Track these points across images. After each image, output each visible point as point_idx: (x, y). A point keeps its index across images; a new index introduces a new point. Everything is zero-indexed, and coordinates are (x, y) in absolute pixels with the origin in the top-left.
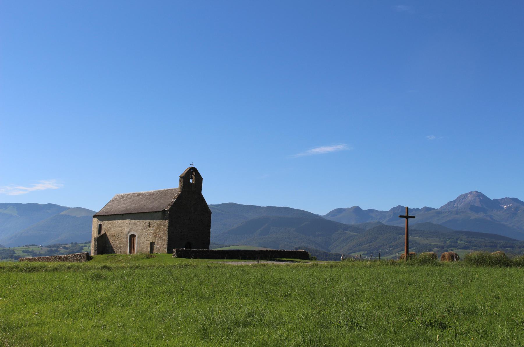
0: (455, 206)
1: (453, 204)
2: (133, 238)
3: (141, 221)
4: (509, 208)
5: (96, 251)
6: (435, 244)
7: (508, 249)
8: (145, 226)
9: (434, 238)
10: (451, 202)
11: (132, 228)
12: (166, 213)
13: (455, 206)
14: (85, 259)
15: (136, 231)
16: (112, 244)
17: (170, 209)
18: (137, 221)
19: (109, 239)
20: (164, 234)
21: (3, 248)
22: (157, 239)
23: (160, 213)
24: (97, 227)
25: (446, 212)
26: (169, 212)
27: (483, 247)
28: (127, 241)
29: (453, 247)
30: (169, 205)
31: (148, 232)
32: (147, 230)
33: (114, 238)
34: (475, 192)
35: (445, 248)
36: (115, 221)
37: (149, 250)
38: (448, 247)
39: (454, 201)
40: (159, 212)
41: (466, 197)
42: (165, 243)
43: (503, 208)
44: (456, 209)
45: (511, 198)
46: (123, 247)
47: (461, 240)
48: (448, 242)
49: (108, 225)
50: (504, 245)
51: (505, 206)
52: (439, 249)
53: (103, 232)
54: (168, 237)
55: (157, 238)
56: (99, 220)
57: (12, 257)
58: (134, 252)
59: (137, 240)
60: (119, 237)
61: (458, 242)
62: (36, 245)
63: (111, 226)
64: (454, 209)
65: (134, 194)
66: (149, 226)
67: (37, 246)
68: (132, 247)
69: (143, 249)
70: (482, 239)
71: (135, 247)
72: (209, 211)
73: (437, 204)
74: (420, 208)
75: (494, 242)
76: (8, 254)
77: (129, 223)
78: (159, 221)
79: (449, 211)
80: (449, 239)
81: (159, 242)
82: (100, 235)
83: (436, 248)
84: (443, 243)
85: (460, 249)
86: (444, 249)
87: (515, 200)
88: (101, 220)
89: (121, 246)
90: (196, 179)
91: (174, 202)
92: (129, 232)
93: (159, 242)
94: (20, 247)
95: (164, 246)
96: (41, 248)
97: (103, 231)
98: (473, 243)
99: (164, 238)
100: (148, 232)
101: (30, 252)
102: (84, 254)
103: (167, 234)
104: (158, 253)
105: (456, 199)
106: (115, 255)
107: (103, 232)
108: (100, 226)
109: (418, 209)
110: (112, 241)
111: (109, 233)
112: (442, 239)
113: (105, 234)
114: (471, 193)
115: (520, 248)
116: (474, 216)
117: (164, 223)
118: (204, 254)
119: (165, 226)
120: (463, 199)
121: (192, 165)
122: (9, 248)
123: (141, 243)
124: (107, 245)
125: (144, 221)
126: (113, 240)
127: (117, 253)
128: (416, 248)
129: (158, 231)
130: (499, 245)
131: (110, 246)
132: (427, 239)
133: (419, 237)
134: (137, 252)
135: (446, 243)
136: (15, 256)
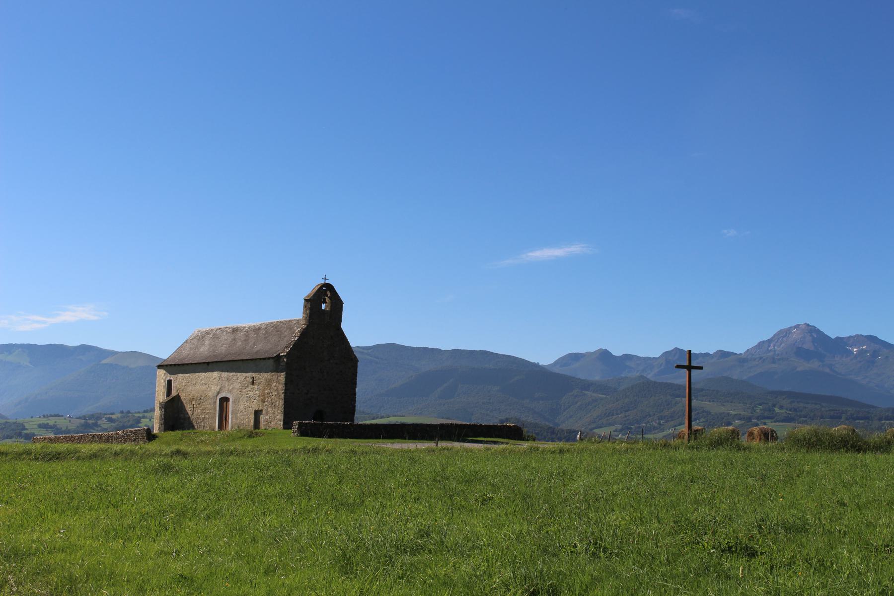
0: (771, 350)
2: (225, 403)
4: (861, 352)
5: (163, 426)
6: (736, 413)
7: (859, 423)
11: (223, 386)
12: (282, 360)
15: (230, 391)
16: (190, 414)
17: (288, 353)
19: (185, 405)
20: (278, 396)
22: (266, 405)
23: (271, 361)
25: (755, 359)
26: (285, 360)
29: (768, 418)
31: (251, 393)
32: (249, 389)
33: (193, 402)
34: (804, 326)
35: (753, 420)
37: (252, 423)
38: (758, 418)
39: (769, 341)
40: (269, 358)
41: (789, 334)
42: (279, 412)
43: (852, 352)
44: (772, 353)
46: (208, 418)
47: (781, 407)
49: (183, 381)
51: (855, 350)
52: (743, 422)
53: (174, 393)
55: (266, 403)
57: (20, 435)
58: (227, 426)
63: (188, 383)
66: (253, 383)
67: (62, 416)
68: (224, 418)
69: (243, 422)
70: (816, 404)
73: (740, 345)
74: (711, 353)
75: (836, 410)
77: (218, 378)
79: (761, 358)
80: (760, 404)
81: (270, 409)
83: (738, 420)
84: (750, 411)
85: (779, 421)
86: (751, 421)
87: (872, 339)
88: (171, 373)
90: (332, 303)
92: (218, 393)
93: (270, 409)
96: (70, 421)
97: (175, 391)
99: (277, 402)
100: (251, 393)
101: (51, 427)
103: (282, 396)
105: (773, 338)
107: (174, 393)
108: (170, 382)
109: (707, 354)
112: (748, 405)
114: (797, 326)
115: (880, 419)
116: (803, 366)
117: (277, 377)
119: (279, 383)
120: (783, 337)
122: (15, 421)
123: (239, 412)
124: (182, 415)
125: (244, 374)
126: (191, 406)
128: (704, 420)
130: (844, 415)
131: (186, 416)
133: (710, 401)
134: (232, 427)
135: (755, 411)
136: (26, 434)
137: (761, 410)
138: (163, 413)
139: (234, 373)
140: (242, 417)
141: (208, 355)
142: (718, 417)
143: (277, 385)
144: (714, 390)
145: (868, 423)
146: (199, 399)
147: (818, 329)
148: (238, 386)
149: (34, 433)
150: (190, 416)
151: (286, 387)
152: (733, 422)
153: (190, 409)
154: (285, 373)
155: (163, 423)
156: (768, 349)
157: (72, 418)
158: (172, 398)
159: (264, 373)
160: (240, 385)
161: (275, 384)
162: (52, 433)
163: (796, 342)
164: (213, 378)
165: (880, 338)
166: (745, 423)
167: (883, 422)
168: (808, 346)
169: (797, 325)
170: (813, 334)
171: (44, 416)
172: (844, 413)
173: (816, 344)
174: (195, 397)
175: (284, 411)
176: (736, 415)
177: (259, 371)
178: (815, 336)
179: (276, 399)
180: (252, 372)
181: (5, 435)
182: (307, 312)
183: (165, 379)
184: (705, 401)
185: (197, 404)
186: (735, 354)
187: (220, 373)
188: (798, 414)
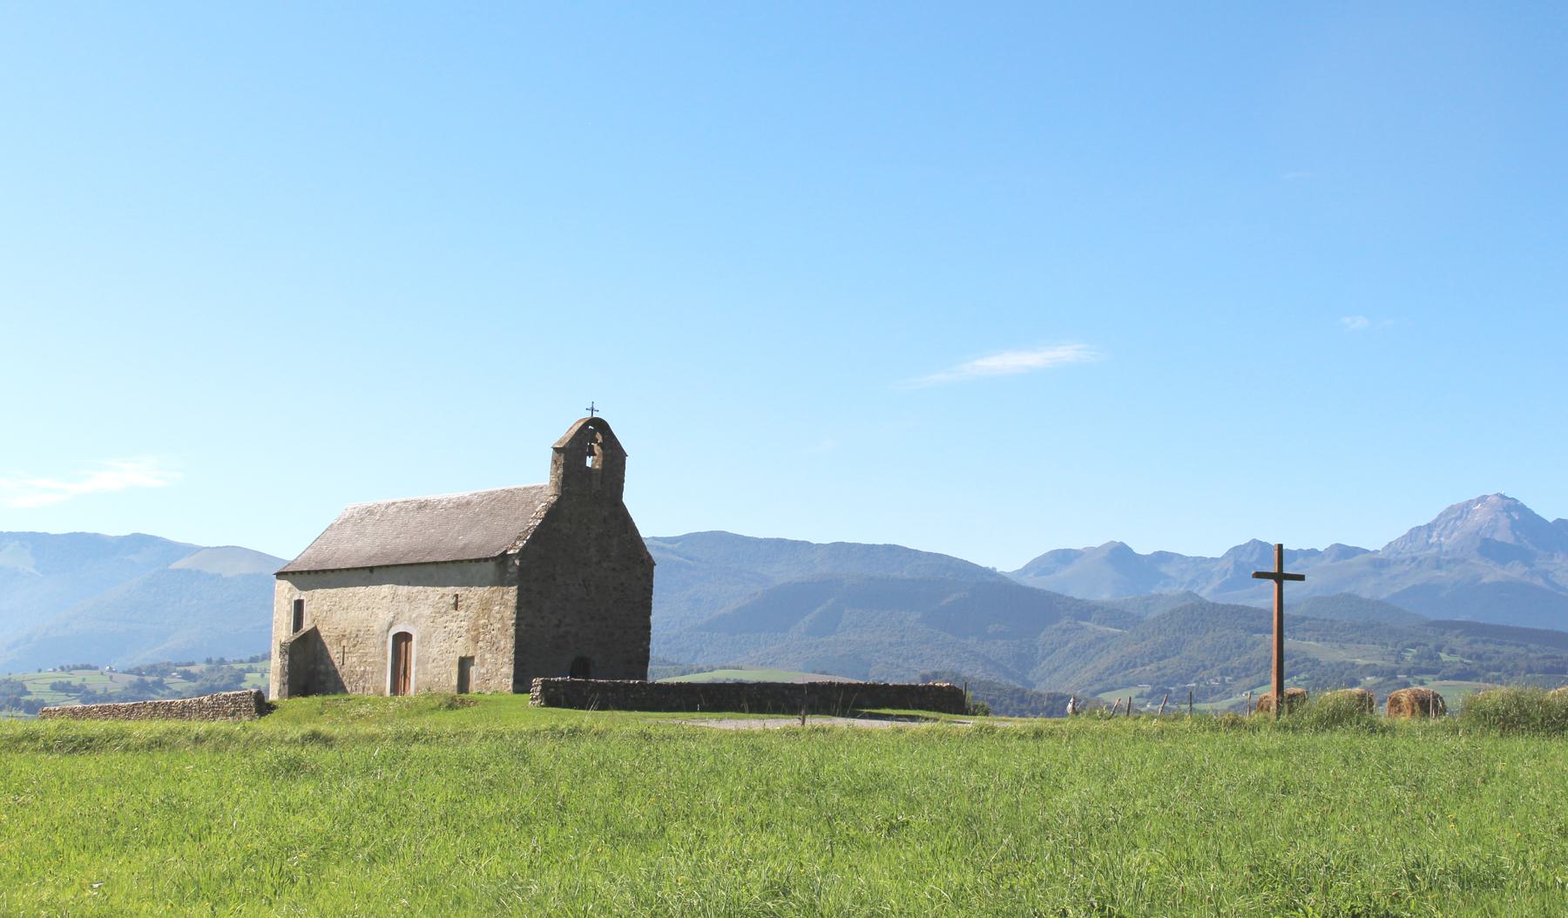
0: (1433, 543)
2: (404, 644)
3: (430, 589)
5: (287, 686)
6: (1367, 662)
12: (510, 563)
15: (413, 622)
16: (337, 664)
17: (523, 550)
19: (328, 647)
20: (504, 629)
24: (288, 608)
26: (517, 562)
27: (1523, 672)
28: (385, 654)
29: (1427, 672)
31: (453, 626)
33: (344, 643)
37: (455, 682)
38: (1408, 672)
39: (1430, 527)
40: (486, 560)
41: (1468, 513)
42: (507, 660)
44: (1434, 550)
46: (372, 673)
47: (1452, 652)
48: (1410, 656)
49: (324, 602)
52: (1381, 679)
53: (307, 626)
54: (516, 641)
55: (480, 644)
56: (294, 588)
57: (16, 704)
59: (418, 650)
61: (1443, 655)
62: (93, 665)
63: (334, 605)
64: (1428, 552)
66: (456, 606)
67: (96, 668)
68: (402, 673)
69: (437, 679)
70: (1518, 646)
71: (410, 673)
73: (1375, 536)
74: (1321, 549)
77: (390, 597)
78: (486, 589)
79: (1414, 559)
80: (1413, 646)
81: (488, 656)
84: (1393, 659)
86: (1397, 678)
88: (302, 588)
90: (605, 455)
91: (536, 530)
92: (391, 625)
93: (488, 656)
94: (42, 674)
96: (111, 677)
97: (309, 622)
99: (502, 643)
100: (453, 626)
101: (76, 690)
102: (246, 694)
103: (512, 631)
105: (1437, 520)
106: (346, 697)
107: (307, 626)
108: (299, 605)
109: (1313, 552)
111: (327, 629)
113: (315, 632)
114: (1483, 499)
116: (1493, 573)
117: (503, 595)
120: (1456, 519)
122: (7, 677)
123: (431, 660)
124: (322, 667)
126: (340, 649)
128: (1307, 676)
129: (482, 622)
131: (330, 668)
133: (1317, 640)
134: (417, 689)
135: (1403, 659)
136: (28, 702)
137: (1414, 657)
138: (287, 662)
140: (436, 671)
146: (354, 635)
149: (43, 700)
151: (518, 614)
152: (1362, 680)
154: (516, 587)
155: (286, 681)
157: (116, 671)
160: (431, 609)
162: (78, 700)
164: (382, 596)
166: (1383, 681)
168: (1503, 536)
169: (1484, 496)
171: (62, 669)
173: (1518, 533)
174: (348, 631)
177: (469, 584)
178: (1517, 518)
179: (499, 637)
183: (292, 597)
185: (350, 645)
186: (1365, 551)
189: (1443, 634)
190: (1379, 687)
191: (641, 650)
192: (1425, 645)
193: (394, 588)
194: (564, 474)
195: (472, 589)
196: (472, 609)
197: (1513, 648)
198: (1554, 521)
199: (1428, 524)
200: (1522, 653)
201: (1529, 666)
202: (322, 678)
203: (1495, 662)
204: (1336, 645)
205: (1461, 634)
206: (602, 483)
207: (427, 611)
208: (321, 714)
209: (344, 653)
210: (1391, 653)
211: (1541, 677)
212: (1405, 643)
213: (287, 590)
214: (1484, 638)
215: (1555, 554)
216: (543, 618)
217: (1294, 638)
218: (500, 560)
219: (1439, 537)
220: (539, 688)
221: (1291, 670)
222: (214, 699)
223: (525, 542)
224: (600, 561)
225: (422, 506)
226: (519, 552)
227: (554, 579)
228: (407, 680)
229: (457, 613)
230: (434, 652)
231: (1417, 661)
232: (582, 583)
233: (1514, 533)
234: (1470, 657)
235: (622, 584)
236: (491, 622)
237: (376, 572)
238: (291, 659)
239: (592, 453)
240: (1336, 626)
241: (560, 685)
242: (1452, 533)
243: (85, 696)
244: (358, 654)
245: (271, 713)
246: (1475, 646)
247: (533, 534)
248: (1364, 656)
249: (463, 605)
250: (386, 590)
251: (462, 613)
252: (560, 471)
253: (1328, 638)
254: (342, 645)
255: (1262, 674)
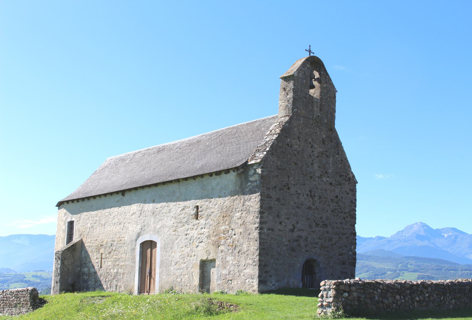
0: (403, 236)
1: (401, 233)
2: (149, 250)
3: (172, 204)
4: (449, 237)
5: (59, 284)
6: (388, 268)
7: (451, 272)
8: (183, 216)
9: (387, 263)
10: (400, 231)
11: (146, 223)
12: (252, 172)
13: (403, 235)
14: (26, 304)
15: (158, 232)
16: (96, 267)
17: (264, 160)
18: (159, 205)
19: (90, 254)
20: (247, 233)
21: (15, 273)
22: (222, 251)
23: (232, 176)
24: (64, 227)
25: (396, 240)
26: (259, 171)
27: (431, 270)
28: (134, 259)
29: (405, 270)
30: (258, 151)
31: (194, 233)
32: (189, 227)
33: (102, 251)
34: (420, 223)
35: (397, 271)
36: (105, 210)
37: (196, 281)
38: (399, 270)
39: (402, 231)
40: (227, 171)
41: (412, 227)
42: (251, 262)
43: (444, 237)
44: (404, 237)
45: (450, 227)
46: (123, 274)
47: (411, 265)
48: (400, 266)
49: (88, 221)
50: (448, 268)
51: (446, 235)
52: (392, 272)
53: (76, 239)
54: (260, 244)
55: (222, 248)
56: (68, 213)
57: (22, 281)
58: (152, 286)
59: (161, 255)
60: (114, 248)
61: (408, 266)
62: (44, 270)
63: (95, 223)
64: (402, 238)
65: (149, 151)
66: (197, 216)
67: (44, 271)
68: (147, 274)
69: (179, 280)
70: (428, 263)
71: (155, 274)
72: (351, 175)
73: (388, 233)
74: (373, 237)
75: (439, 266)
76: (19, 278)
77: (138, 213)
78: (227, 198)
79: (399, 240)
80: (400, 263)
81: (229, 258)
82: (70, 245)
83: (389, 271)
84: (395, 267)
85: (410, 272)
86: (397, 272)
87: (454, 230)
88: (73, 212)
89: (118, 270)
90: (322, 88)
91: (273, 144)
92: (138, 236)
93: (229, 258)
94: (30, 273)
95: (247, 271)
96: (48, 273)
97: (77, 237)
98: (421, 267)
99: (245, 246)
100: (194, 233)
101: (39, 277)
102: (24, 291)
103: (256, 234)
104: (226, 290)
105: (404, 229)
106: (103, 294)
107: (76, 239)
108: (71, 224)
109: (371, 238)
110: (97, 258)
111: (89, 241)
112: (394, 264)
113: (81, 243)
114: (416, 223)
115: (462, 270)
116: (420, 243)
117: (244, 202)
118: (417, 299)
119: (248, 212)
120: (410, 229)
121: (310, 51)
122: (20, 274)
123: (173, 263)
124: (86, 270)
125: (180, 203)
126: (99, 256)
127: (107, 288)
128: (372, 272)
129: (223, 228)
130: (443, 268)
131: (92, 270)
132: (382, 264)
133: (374, 262)
134: (161, 288)
135: (398, 267)
136: (26, 280)
137: (401, 266)
138: (59, 266)
139: (164, 204)
140: (178, 272)
141: (124, 183)
142: (379, 270)
143: (244, 215)
144: (376, 256)
145: (456, 272)
146: (110, 245)
147: (427, 225)
148: (170, 223)
149: (29, 280)
150: (97, 270)
151: (261, 218)
152: (387, 273)
153: (97, 261)
154: (259, 194)
155: (58, 280)
156: (402, 235)
157: (50, 272)
158: (73, 245)
159: (217, 199)
160: (173, 220)
161: (238, 214)
162: (39, 280)
163: (416, 231)
164: (132, 212)
165: (458, 229)
166: (393, 273)
167: (464, 272)
168: (422, 233)
169: (416, 223)
170: (424, 227)
171: (35, 271)
172: (444, 267)
173: (426, 232)
174: (105, 242)
175: (260, 260)
176: (388, 269)
177: (209, 196)
178: (426, 228)
179: (241, 241)
180: (195, 199)
181: (15, 281)
182: (288, 97)
183: (66, 219)
184: (372, 262)
185: (107, 252)
186: (385, 238)
187: (142, 205)
188: (420, 268)
189: (408, 260)
190: (392, 275)
191: (351, 253)
192: (403, 263)
193: (141, 206)
194: (294, 98)
195: (213, 200)
196: (212, 217)
197: (427, 263)
198: (436, 229)
199: (402, 230)
200: (430, 265)
201: (432, 269)
202: (85, 277)
203: (423, 268)
204: (380, 263)
205: (413, 260)
206: (321, 110)
207: (170, 222)
208: (78, 311)
209: (102, 258)
210: (394, 265)
211: (436, 271)
212: (398, 262)
213: (63, 215)
214: (419, 261)
215: (436, 238)
216: (280, 223)
217: (368, 261)
218: (241, 170)
219: (405, 234)
220: (332, 293)
221: (368, 270)
222: (4, 294)
223: (265, 153)
224: (321, 175)
225: (160, 150)
226: (261, 161)
227: (289, 189)
228: (152, 280)
229: (198, 221)
230: (177, 256)
231: (402, 267)
232: (309, 194)
233: (425, 233)
234: (416, 266)
235: (337, 197)
236: (232, 227)
237: (127, 195)
238: (62, 263)
239: (313, 87)
240: (379, 258)
241: (353, 288)
242: (408, 232)
243: (41, 279)
244: (113, 259)
245: (41, 307)
246: (417, 263)
247: (271, 147)
248: (387, 266)
249: (202, 215)
250: (135, 208)
251: (202, 221)
252: (291, 95)
253: (377, 261)
254: (100, 253)
255: (360, 271)
